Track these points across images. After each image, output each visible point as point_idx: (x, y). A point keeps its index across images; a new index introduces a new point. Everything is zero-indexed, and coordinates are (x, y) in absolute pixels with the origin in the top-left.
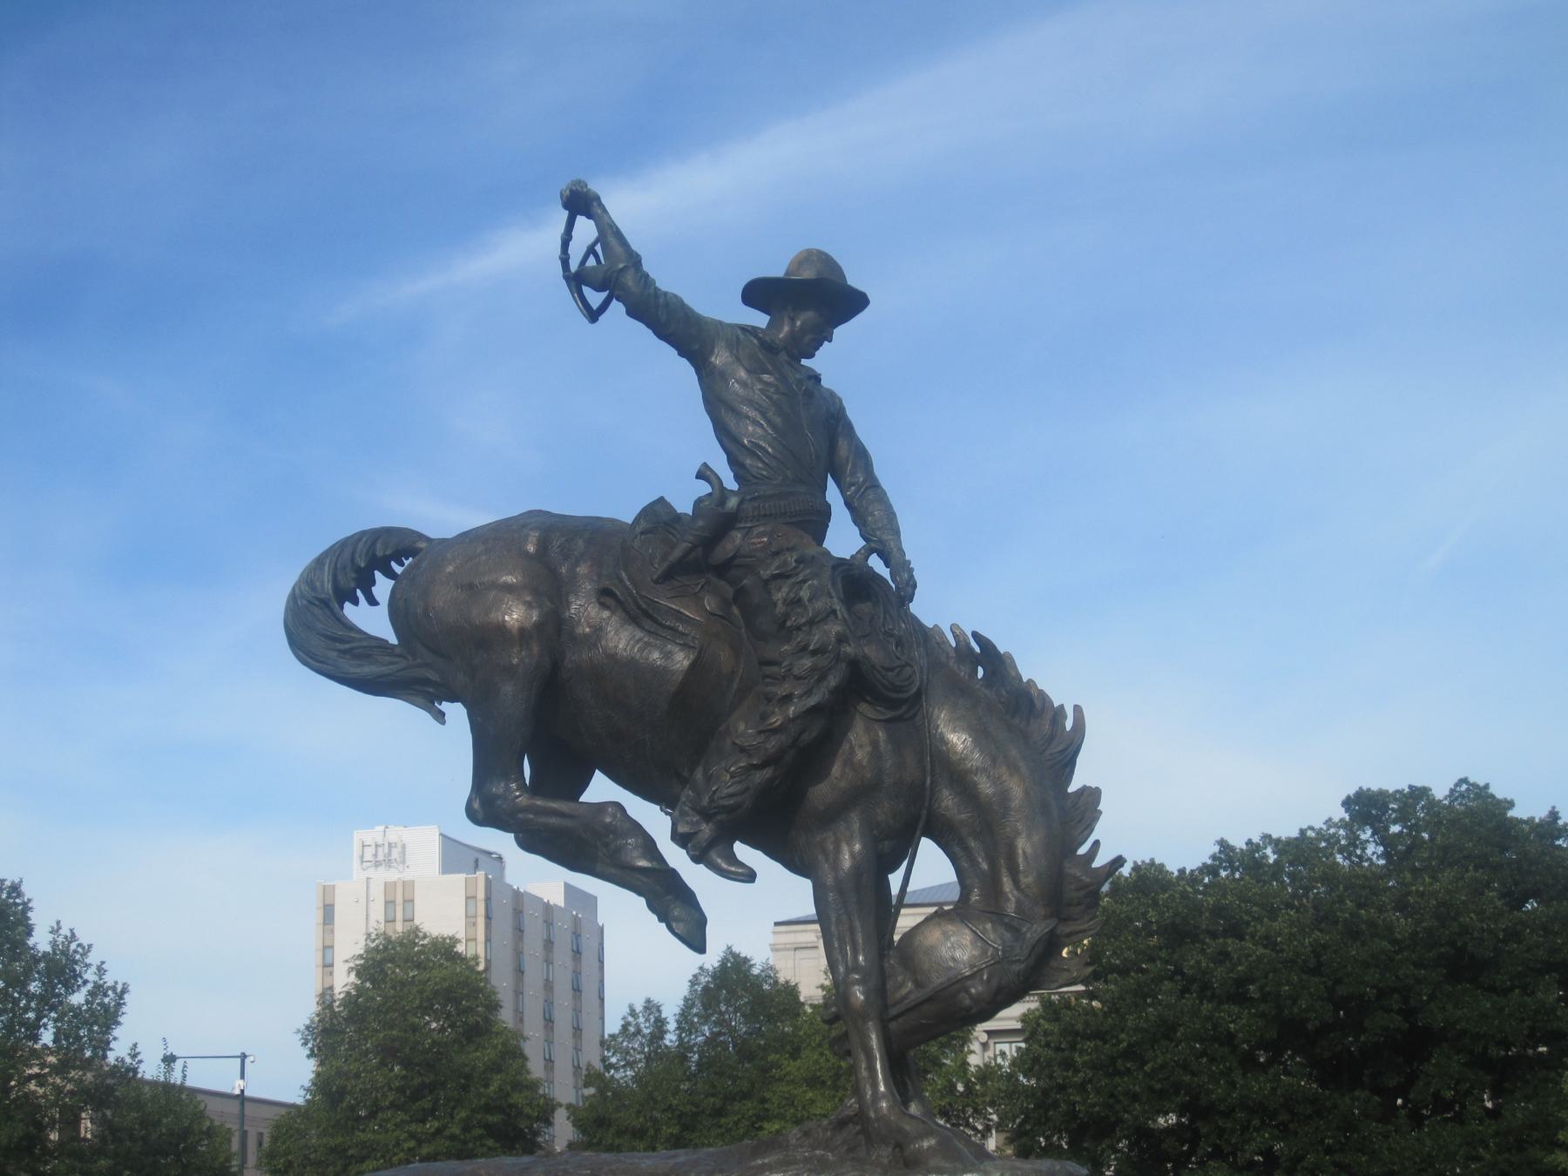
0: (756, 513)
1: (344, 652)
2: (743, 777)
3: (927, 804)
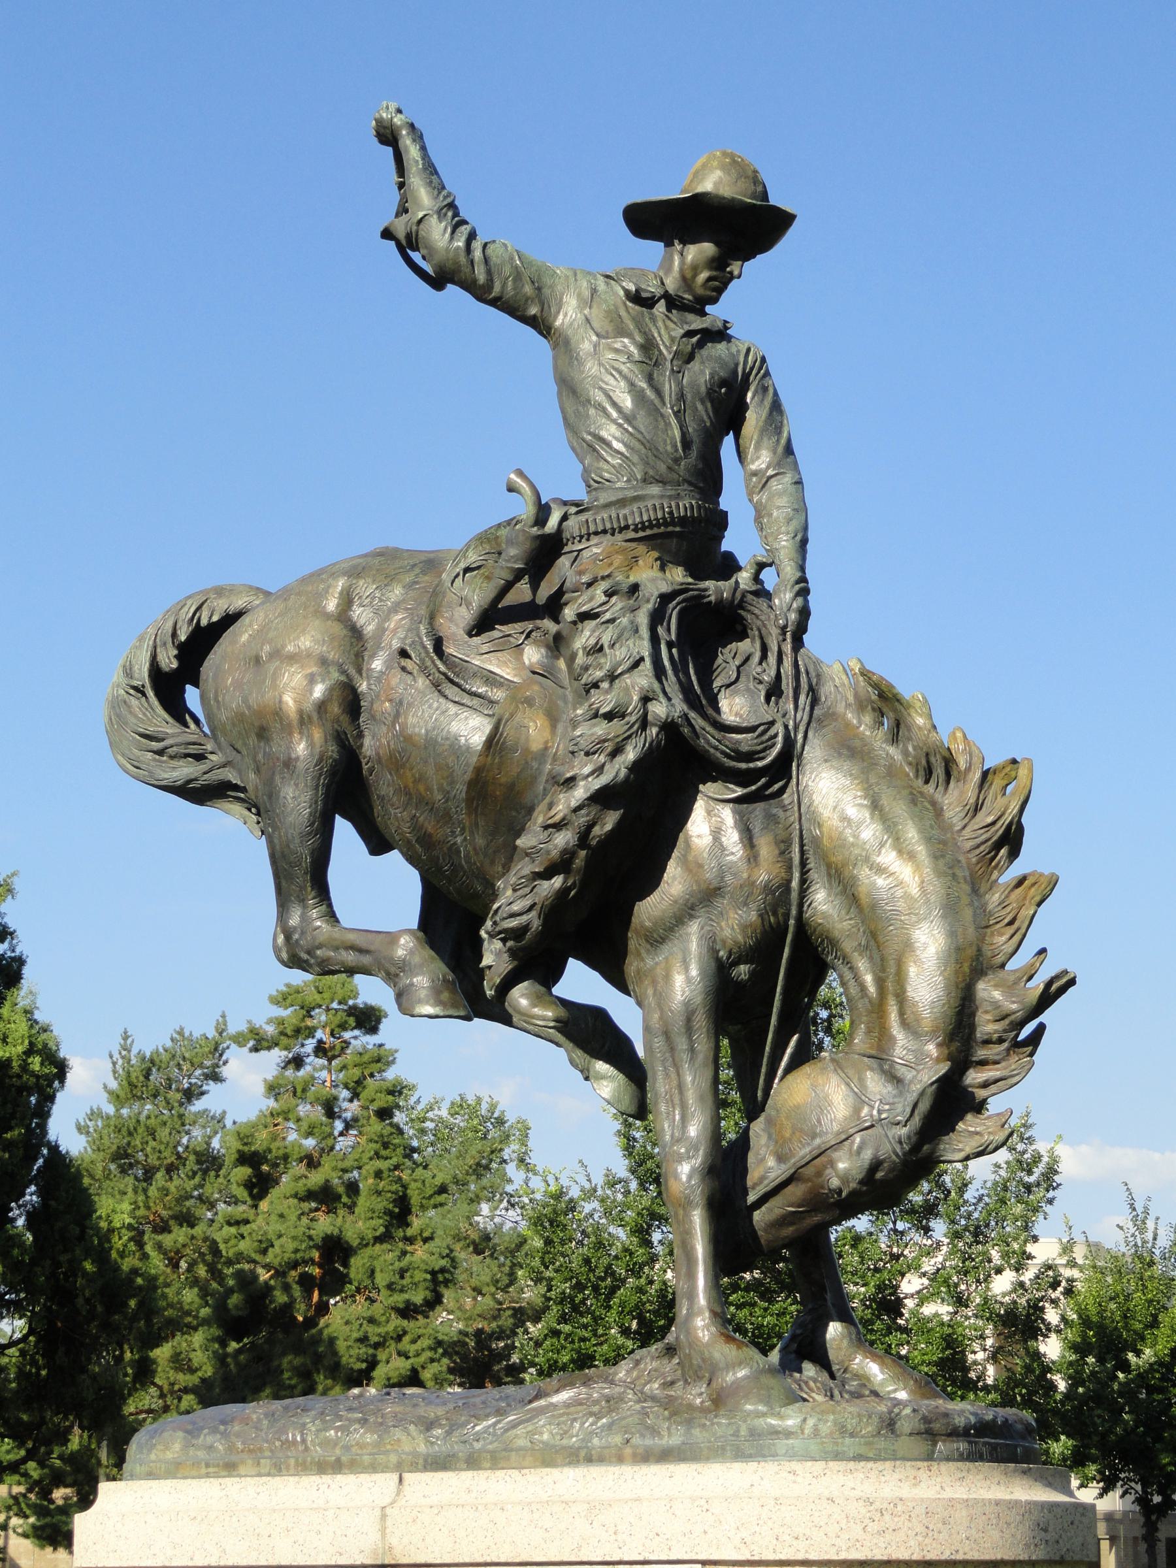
0: (584, 531)
1: (160, 753)
2: (527, 890)
3: (794, 912)
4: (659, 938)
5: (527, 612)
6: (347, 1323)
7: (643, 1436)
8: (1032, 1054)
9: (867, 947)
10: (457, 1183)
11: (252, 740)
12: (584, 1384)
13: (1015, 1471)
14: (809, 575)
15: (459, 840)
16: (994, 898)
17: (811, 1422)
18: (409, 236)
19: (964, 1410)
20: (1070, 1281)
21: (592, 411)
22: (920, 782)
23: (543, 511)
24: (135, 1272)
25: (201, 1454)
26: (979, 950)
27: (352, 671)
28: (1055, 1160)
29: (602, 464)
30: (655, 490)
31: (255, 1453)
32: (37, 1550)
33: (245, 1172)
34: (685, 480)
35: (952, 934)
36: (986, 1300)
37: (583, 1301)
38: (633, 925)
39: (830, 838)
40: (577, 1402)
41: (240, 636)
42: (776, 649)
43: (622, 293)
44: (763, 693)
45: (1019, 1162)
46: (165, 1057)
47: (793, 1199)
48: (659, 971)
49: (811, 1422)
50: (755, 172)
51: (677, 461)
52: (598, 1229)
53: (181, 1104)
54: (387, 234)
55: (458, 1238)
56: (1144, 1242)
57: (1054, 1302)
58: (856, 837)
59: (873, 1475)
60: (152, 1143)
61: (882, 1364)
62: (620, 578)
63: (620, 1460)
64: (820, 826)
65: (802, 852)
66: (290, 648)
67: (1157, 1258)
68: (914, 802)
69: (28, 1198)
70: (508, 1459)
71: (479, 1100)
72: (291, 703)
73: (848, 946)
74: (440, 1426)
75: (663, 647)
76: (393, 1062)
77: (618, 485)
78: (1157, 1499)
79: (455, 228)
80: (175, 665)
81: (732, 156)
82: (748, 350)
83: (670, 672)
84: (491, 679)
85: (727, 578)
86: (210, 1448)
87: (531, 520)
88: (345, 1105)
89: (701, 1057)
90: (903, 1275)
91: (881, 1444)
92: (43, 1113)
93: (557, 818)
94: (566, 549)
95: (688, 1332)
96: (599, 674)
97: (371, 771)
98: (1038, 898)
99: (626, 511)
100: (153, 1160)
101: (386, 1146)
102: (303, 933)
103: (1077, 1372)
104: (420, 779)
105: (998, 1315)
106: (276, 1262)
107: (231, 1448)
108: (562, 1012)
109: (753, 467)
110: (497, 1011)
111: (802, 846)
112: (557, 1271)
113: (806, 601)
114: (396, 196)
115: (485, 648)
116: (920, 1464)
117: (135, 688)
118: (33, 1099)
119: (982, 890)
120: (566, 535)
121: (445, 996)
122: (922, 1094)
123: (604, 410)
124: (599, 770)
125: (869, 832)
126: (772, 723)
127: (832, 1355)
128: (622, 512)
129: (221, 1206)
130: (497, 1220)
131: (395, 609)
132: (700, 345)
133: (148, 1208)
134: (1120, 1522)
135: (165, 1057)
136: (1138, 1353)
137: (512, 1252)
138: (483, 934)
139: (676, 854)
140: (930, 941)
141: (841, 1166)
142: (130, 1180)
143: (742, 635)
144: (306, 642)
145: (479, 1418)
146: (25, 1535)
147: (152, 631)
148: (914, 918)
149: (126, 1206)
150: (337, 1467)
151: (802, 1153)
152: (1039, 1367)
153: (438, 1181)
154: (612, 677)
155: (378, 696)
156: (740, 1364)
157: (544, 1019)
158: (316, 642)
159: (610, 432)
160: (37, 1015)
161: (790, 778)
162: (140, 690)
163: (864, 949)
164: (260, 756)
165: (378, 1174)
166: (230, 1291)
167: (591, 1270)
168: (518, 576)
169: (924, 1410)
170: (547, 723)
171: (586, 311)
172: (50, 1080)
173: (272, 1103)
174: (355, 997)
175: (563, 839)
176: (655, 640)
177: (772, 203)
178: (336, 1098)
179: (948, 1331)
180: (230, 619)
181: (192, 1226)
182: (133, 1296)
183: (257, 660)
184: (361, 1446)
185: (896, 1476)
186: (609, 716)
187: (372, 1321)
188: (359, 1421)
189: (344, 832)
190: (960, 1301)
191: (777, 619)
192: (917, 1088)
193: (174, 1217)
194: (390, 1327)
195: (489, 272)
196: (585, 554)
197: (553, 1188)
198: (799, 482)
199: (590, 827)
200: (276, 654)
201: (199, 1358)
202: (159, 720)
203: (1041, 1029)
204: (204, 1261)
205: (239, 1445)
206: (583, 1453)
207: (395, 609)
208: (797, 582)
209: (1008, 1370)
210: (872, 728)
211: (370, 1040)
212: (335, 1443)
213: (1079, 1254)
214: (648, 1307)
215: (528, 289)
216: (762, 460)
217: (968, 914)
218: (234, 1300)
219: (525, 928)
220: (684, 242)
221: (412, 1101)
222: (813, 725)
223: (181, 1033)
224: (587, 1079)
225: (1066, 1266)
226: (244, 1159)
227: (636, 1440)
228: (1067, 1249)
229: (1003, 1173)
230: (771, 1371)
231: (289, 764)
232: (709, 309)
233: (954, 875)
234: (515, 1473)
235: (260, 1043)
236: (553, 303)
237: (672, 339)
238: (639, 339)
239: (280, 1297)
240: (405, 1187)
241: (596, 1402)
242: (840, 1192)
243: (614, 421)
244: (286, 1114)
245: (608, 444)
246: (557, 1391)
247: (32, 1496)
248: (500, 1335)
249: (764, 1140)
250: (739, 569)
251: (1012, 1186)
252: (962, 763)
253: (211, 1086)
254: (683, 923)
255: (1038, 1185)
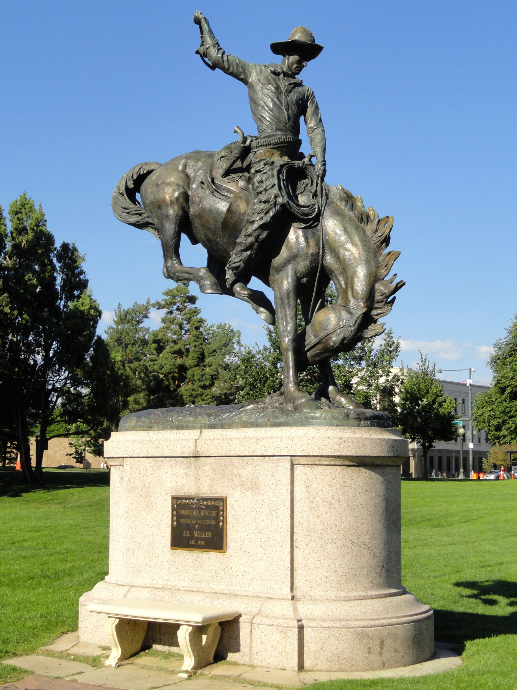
0: (257, 145)
1: (128, 213)
3: (320, 262)
4: (280, 269)
5: (240, 170)
6: (186, 390)
7: (273, 419)
8: (392, 306)
9: (342, 273)
10: (219, 349)
11: (156, 209)
12: (256, 403)
13: (384, 430)
14: (326, 160)
15: (219, 240)
16: (381, 259)
17: (323, 415)
18: (204, 53)
19: (369, 412)
20: (403, 379)
21: (260, 108)
22: (359, 223)
23: (244, 141)
24: (122, 374)
25: (141, 424)
26: (376, 274)
27: (187, 188)
28: (399, 343)
29: (263, 125)
30: (279, 132)
31: (158, 423)
32: (94, 457)
33: (155, 345)
34: (288, 130)
35: (368, 269)
36: (377, 385)
37: (257, 384)
38: (272, 265)
39: (331, 240)
40: (253, 409)
41: (152, 177)
42: (316, 182)
43: (270, 71)
44: (312, 195)
45: (388, 344)
46: (131, 311)
47: (319, 349)
48: (279, 280)
49: (323, 415)
50: (311, 33)
51: (286, 124)
52: (261, 363)
53: (136, 325)
54: (197, 52)
55: (219, 365)
56: (425, 368)
57: (398, 386)
58: (339, 239)
59: (342, 430)
60: (127, 337)
61: (345, 398)
62: (268, 160)
63: (266, 426)
64: (328, 236)
65: (323, 244)
66: (168, 181)
67: (429, 373)
68: (357, 229)
69: (90, 352)
70: (233, 425)
71: (226, 324)
72: (168, 198)
73: (336, 272)
74: (213, 416)
75: (281, 181)
76: (200, 313)
77: (268, 131)
78: (427, 444)
79: (218, 50)
80: (133, 186)
81: (304, 28)
82: (308, 89)
83: (283, 189)
84: (229, 191)
85: (301, 160)
86: (144, 422)
87: (242, 142)
88: (186, 325)
89: (292, 306)
90: (352, 377)
91: (345, 421)
92: (95, 327)
93: (249, 233)
94: (252, 151)
95: (287, 389)
96: (262, 189)
97: (192, 219)
98: (394, 259)
99: (270, 139)
100: (128, 342)
101: (198, 338)
102: (172, 268)
103: (404, 407)
104: (208, 221)
105: (381, 389)
106: (165, 372)
107: (150, 422)
108: (250, 292)
109: (309, 126)
110: (230, 292)
111: (323, 242)
112: (249, 375)
113: (325, 167)
114: (200, 41)
115: (227, 181)
116: (356, 427)
117: (120, 193)
118: (91, 323)
119: (378, 256)
120: (252, 146)
121: (215, 287)
122: (358, 317)
123: (264, 108)
124: (262, 218)
125: (343, 238)
126: (314, 205)
127: (330, 395)
128: (269, 140)
129: (148, 356)
130: (231, 360)
131: (200, 169)
132: (294, 88)
133: (126, 356)
134: (416, 451)
135: (131, 311)
136: (422, 401)
137: (235, 370)
138: (226, 268)
139: (285, 244)
140: (361, 271)
141: (334, 339)
142: (121, 348)
143: (306, 178)
144: (172, 179)
145: (224, 414)
146: (90, 453)
147: (125, 176)
148: (357, 264)
149: (120, 355)
150: (182, 428)
151: (322, 335)
152: (393, 405)
153: (213, 349)
154: (266, 190)
155: (194, 196)
156: (303, 398)
157: (244, 294)
158: (176, 179)
159: (266, 115)
160: (92, 297)
161: (320, 221)
162: (122, 194)
163: (341, 274)
164: (159, 214)
165: (195, 346)
166: (151, 381)
167: (259, 375)
168: (237, 159)
169: (357, 412)
170: (246, 204)
171: (259, 77)
172: (96, 317)
173: (163, 325)
174: (188, 293)
175: (251, 239)
176: (279, 179)
177: (316, 43)
178: (183, 323)
179: (365, 394)
180: (149, 172)
181: (140, 361)
182: (122, 382)
183: (158, 185)
184: (189, 421)
185: (349, 431)
186: (265, 202)
187: (193, 390)
188: (189, 414)
189: (184, 237)
190: (370, 385)
191: (316, 173)
192: (357, 316)
193: (134, 359)
194: (199, 392)
195: (229, 64)
196: (258, 152)
197: (247, 351)
198: (323, 131)
199: (259, 236)
200: (163, 183)
201: (142, 400)
202: (128, 203)
203: (394, 298)
204: (143, 372)
205: (153, 421)
206: (255, 424)
207: (200, 169)
208: (323, 161)
209: (384, 406)
210: (345, 206)
211: (193, 306)
212: (181, 421)
213: (405, 371)
214: (276, 386)
215: (241, 70)
216: (312, 124)
217: (373, 263)
218: (152, 383)
219: (238, 267)
220: (289, 55)
221: (206, 324)
222: (327, 205)
223: (136, 303)
224: (257, 313)
225: (401, 375)
226: (155, 341)
227: (271, 420)
228: (402, 370)
229: (383, 347)
230: (312, 400)
231: (167, 216)
232: (296, 76)
233: (369, 251)
234: (235, 429)
235: (160, 306)
236: (248, 74)
237: (285, 86)
238: (275, 86)
239: (166, 383)
240: (203, 350)
241: (259, 409)
242: (333, 346)
243: (267, 111)
244: (167, 328)
245: (265, 118)
246: (248, 406)
247: (92, 441)
248: (231, 394)
249: (310, 331)
250: (305, 157)
251: (386, 351)
252: (372, 217)
253: (145, 320)
254: (287, 266)
255: (393, 351)
